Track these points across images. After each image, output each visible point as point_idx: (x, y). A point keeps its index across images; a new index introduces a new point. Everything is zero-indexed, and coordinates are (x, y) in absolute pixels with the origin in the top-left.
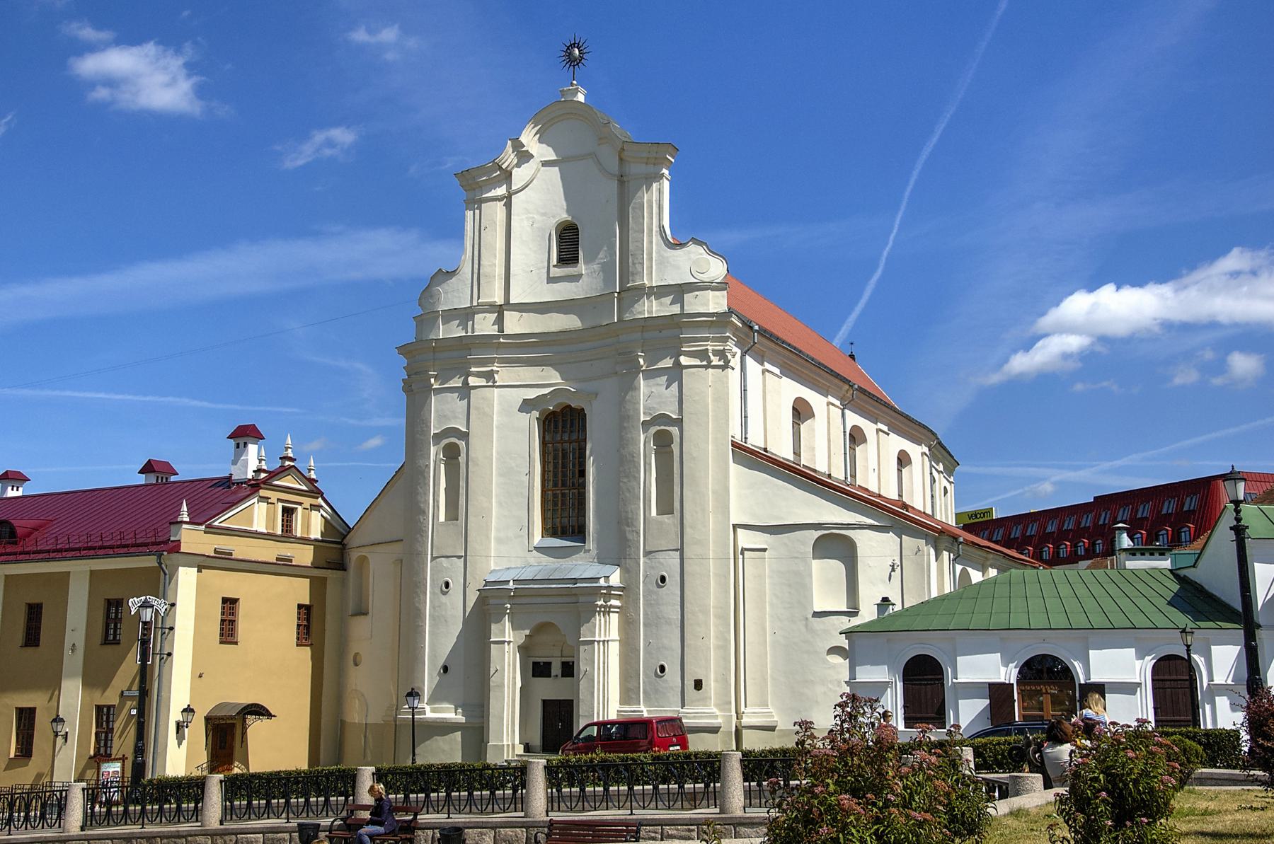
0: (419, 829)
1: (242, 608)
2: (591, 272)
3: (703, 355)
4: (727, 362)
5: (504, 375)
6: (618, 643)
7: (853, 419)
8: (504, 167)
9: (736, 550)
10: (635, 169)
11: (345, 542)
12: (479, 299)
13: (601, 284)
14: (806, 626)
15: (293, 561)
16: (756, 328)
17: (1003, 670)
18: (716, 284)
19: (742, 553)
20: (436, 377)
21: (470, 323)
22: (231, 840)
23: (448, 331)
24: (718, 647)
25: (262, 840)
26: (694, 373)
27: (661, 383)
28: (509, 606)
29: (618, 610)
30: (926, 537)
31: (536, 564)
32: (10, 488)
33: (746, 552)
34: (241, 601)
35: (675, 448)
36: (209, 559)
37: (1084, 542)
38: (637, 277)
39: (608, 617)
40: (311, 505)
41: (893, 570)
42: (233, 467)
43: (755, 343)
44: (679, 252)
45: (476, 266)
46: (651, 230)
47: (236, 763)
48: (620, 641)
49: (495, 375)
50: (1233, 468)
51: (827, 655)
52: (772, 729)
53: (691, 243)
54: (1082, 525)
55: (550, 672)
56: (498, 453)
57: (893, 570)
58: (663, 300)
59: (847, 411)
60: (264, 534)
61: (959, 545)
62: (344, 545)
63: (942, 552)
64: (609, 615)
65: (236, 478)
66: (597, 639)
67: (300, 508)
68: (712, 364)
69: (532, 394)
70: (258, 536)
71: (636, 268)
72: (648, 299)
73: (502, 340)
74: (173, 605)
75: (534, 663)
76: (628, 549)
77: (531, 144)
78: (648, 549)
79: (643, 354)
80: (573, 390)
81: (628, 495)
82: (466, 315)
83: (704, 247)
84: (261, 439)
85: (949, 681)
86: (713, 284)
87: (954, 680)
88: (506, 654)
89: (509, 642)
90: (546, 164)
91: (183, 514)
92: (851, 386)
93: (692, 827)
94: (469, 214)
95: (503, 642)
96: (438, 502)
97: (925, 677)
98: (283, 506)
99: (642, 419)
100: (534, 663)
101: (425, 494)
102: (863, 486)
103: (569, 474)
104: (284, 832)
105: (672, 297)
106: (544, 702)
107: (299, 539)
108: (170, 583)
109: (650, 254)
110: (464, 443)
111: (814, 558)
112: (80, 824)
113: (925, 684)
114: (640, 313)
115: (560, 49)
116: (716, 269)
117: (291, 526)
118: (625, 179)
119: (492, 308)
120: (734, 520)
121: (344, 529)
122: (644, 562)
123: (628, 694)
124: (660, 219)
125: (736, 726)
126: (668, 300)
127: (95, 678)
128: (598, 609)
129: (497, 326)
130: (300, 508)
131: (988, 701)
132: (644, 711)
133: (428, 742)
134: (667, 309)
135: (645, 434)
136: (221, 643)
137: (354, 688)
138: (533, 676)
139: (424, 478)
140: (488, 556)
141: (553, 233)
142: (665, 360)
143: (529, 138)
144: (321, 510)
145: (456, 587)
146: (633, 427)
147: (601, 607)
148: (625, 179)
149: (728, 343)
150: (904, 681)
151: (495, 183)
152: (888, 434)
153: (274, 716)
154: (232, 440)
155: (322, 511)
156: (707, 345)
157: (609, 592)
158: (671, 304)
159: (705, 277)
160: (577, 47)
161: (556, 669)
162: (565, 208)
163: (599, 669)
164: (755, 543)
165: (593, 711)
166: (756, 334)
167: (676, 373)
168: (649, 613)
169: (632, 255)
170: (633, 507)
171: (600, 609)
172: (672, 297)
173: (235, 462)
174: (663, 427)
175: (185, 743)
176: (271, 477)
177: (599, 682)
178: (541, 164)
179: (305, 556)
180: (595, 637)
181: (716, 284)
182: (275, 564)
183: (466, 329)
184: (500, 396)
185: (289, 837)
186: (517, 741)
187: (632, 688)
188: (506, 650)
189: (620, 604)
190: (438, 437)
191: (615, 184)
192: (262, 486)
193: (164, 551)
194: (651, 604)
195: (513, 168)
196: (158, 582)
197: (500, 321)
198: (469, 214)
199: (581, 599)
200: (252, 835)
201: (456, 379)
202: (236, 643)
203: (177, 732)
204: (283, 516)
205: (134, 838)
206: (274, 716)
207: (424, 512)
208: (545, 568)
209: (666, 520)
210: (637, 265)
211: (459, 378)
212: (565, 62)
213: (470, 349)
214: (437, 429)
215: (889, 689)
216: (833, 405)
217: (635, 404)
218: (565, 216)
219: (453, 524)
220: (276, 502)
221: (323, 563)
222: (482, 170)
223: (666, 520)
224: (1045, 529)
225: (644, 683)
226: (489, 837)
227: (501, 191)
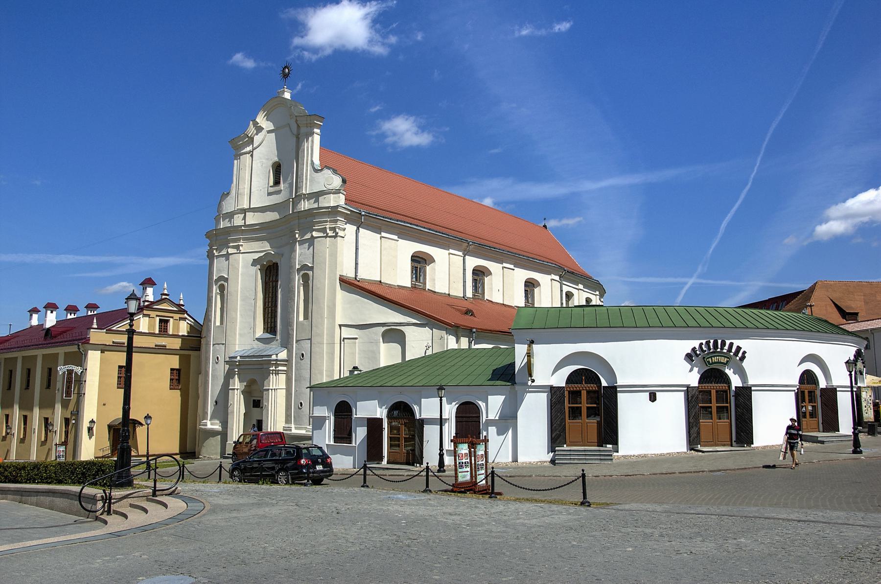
3: (324, 230)
5: (245, 246)
6: (285, 390)
7: (473, 262)
8: (249, 135)
13: (289, 195)
17: (379, 410)
28: (236, 370)
32: (69, 314)
33: (345, 340)
38: (301, 189)
44: (319, 174)
46: (307, 163)
49: (241, 247)
50: (133, 292)
56: (241, 288)
58: (311, 201)
63: (460, 338)
66: (271, 388)
68: (329, 235)
69: (256, 256)
72: (307, 201)
73: (243, 228)
78: (297, 339)
88: (236, 396)
89: (237, 389)
90: (269, 132)
94: (236, 162)
95: (234, 389)
97: (344, 414)
98: (160, 319)
100: (254, 401)
102: (489, 299)
105: (314, 199)
107: (171, 335)
109: (306, 176)
113: (344, 418)
114: (300, 209)
117: (166, 329)
122: (296, 346)
126: (312, 201)
127: (65, 405)
130: (171, 320)
133: (208, 440)
138: (253, 407)
143: (261, 119)
147: (273, 370)
149: (338, 223)
150: (335, 415)
152: (514, 270)
155: (187, 321)
157: (277, 363)
159: (330, 187)
162: (276, 154)
172: (314, 199)
174: (306, 272)
175: (94, 438)
176: (151, 304)
179: (176, 344)
180: (269, 387)
183: (231, 223)
184: (243, 258)
192: (145, 309)
195: (254, 136)
196: (80, 359)
198: (236, 162)
203: (89, 432)
204: (159, 324)
218: (276, 159)
220: (155, 316)
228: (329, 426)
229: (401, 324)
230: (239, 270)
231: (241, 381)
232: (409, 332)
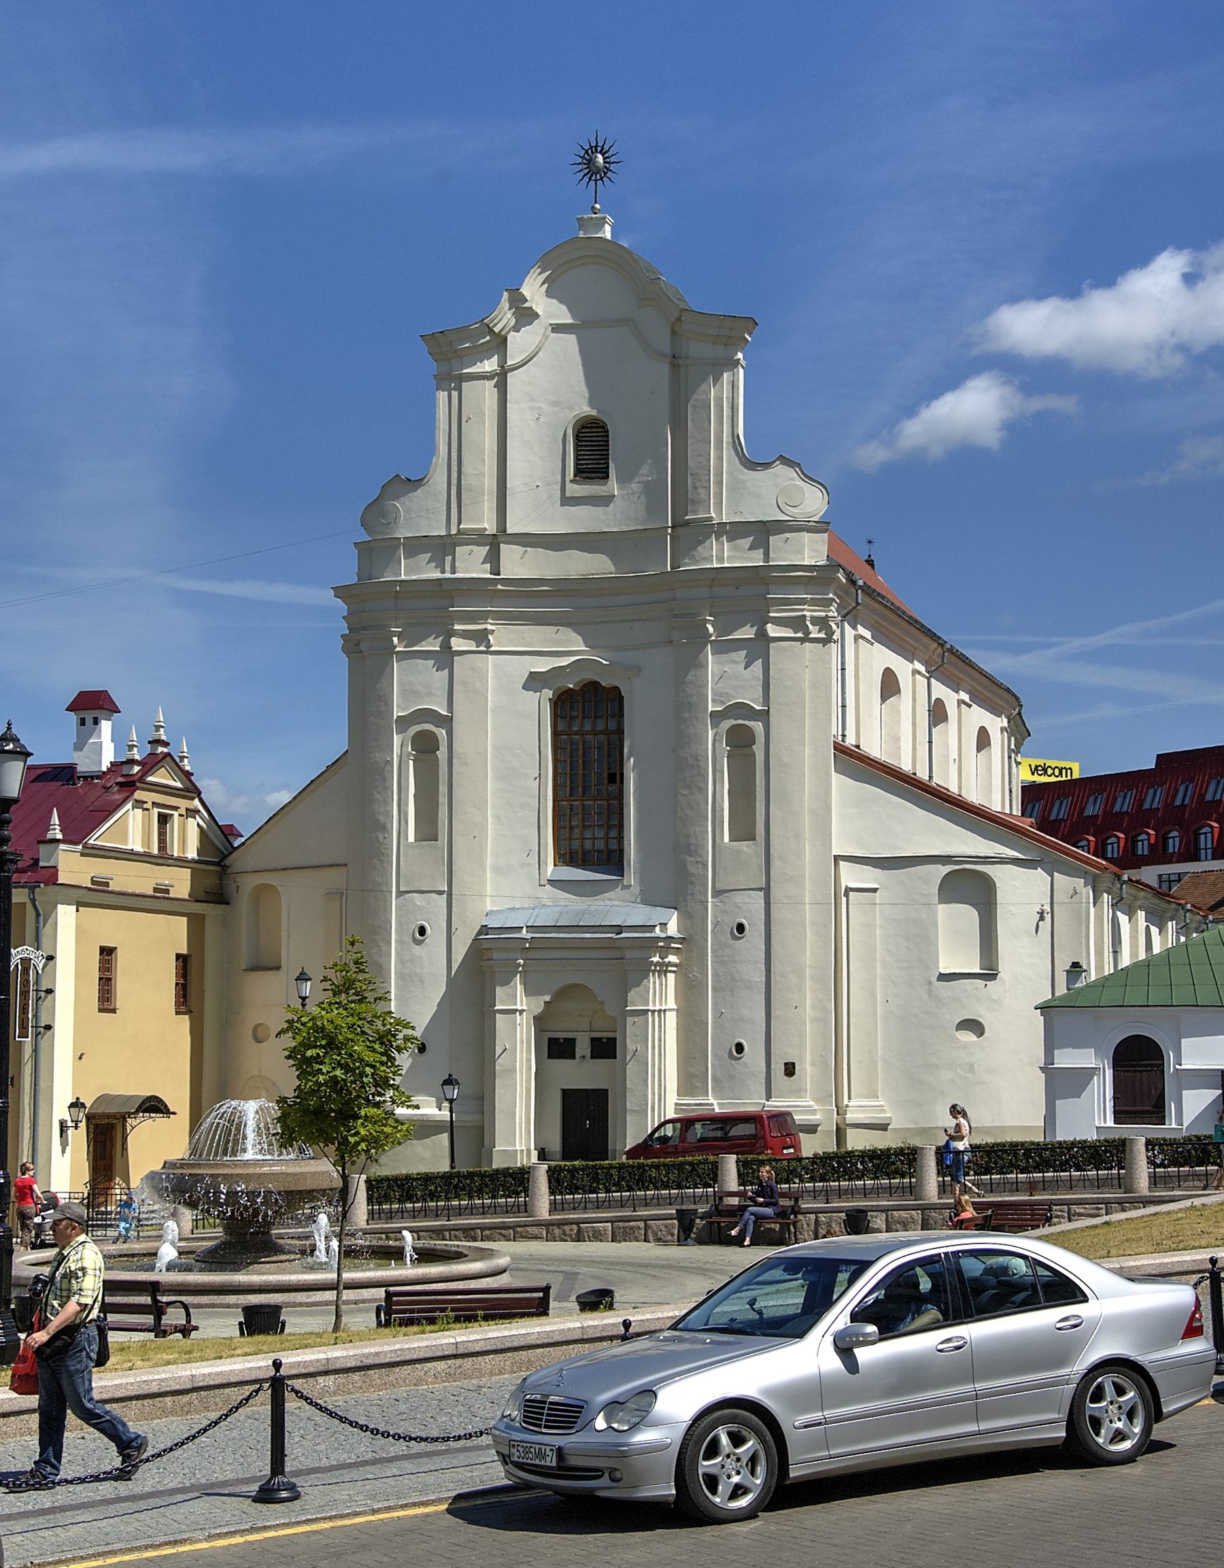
0: (802, 1213)
1: (122, 961)
2: (628, 494)
3: (798, 623)
4: (830, 633)
5: (502, 636)
7: (940, 690)
8: (496, 330)
9: (838, 890)
10: (696, 349)
11: (227, 862)
12: (459, 523)
14: (929, 992)
15: (171, 892)
16: (861, 583)
18: (814, 524)
19: (846, 895)
20: (399, 635)
21: (449, 559)
22: (571, 1230)
23: (408, 570)
24: (815, 1020)
25: (610, 1229)
26: (785, 649)
27: (737, 659)
29: (675, 969)
30: (1084, 874)
31: (551, 904)
33: (851, 893)
34: (118, 949)
35: (759, 750)
36: (91, 893)
37: (1148, 834)
39: (664, 979)
40: (187, 809)
41: (1042, 918)
42: (76, 754)
43: (858, 604)
44: (760, 475)
45: (454, 475)
47: (118, 1180)
48: (677, 1010)
49: (490, 637)
50: (9, 728)
51: (957, 1030)
52: (883, 1127)
53: (778, 462)
54: (1146, 806)
55: (574, 1051)
56: (494, 747)
57: (1042, 918)
58: (739, 542)
59: (933, 680)
60: (138, 854)
61: (1122, 885)
62: (225, 868)
64: (665, 976)
65: (83, 769)
66: (651, 1008)
67: (176, 814)
68: (811, 636)
70: (107, 854)
71: (698, 494)
73: (500, 587)
74: (51, 958)
75: (550, 1040)
76: (690, 887)
77: (536, 298)
78: (719, 886)
79: (712, 619)
80: (605, 662)
81: (689, 812)
82: (442, 548)
83: (797, 469)
84: (116, 712)
85: (1170, 1066)
86: (811, 524)
87: (1178, 1067)
88: (518, 1027)
89: (521, 1012)
90: (557, 328)
91: (55, 829)
92: (942, 646)
93: (1101, 1206)
94: (442, 396)
95: (514, 1011)
96: (406, 814)
99: (710, 709)
101: (386, 802)
103: (593, 778)
104: (638, 1221)
105: (752, 538)
106: (565, 1093)
108: (44, 926)
110: (444, 732)
111: (943, 900)
112: (365, 1217)
115: (573, 155)
116: (813, 502)
118: (681, 362)
119: (480, 538)
120: (835, 852)
121: (221, 843)
123: (690, 1081)
124: (733, 425)
125: (837, 1124)
126: (746, 542)
128: (653, 968)
129: (489, 565)
131: (1221, 1091)
132: (716, 1105)
134: (745, 555)
135: (715, 730)
136: (100, 1010)
137: (257, 1073)
139: (384, 779)
140: (483, 896)
141: (570, 432)
142: (744, 629)
143: (533, 289)
144: (197, 816)
145: (437, 934)
146: (697, 718)
147: (658, 963)
148: (681, 362)
151: (482, 353)
153: (174, 1113)
154: (73, 713)
156: (803, 610)
158: (749, 549)
160: (600, 153)
161: (583, 1047)
162: (587, 395)
163: (653, 1048)
164: (863, 882)
165: (647, 1104)
166: (860, 591)
167: (760, 648)
168: (721, 974)
169: (691, 474)
170: (697, 829)
171: (655, 967)
172: (752, 538)
173: (79, 747)
175: (68, 1149)
177: (653, 1065)
178: (550, 328)
179: (180, 883)
180: (648, 1005)
181: (814, 524)
182: (89, 889)
184: (496, 666)
185: (643, 1225)
186: (533, 1147)
187: (696, 1073)
188: (518, 1022)
189: (678, 961)
190: (404, 723)
191: (665, 368)
192: (138, 784)
193: (40, 882)
194: (723, 962)
195: (508, 332)
197: (494, 558)
198: (442, 396)
199: (628, 954)
200: (599, 1224)
201: (431, 639)
202: (114, 1011)
203: (61, 1136)
205: (446, 1230)
206: (174, 1113)
207: (385, 828)
208: (565, 909)
209: (745, 849)
210: (699, 490)
211: (434, 639)
212: (582, 174)
213: (453, 597)
214: (403, 710)
215: (1095, 1077)
216: (919, 673)
217: (700, 687)
218: (586, 410)
219: (430, 846)
221: (203, 897)
222: (463, 332)
223: (745, 849)
224: (1083, 809)
225: (712, 1065)
226: (881, 1220)
227: (490, 365)
228: (1102, 1089)
229: (986, 860)
230: (487, 697)
231: (528, 992)
232: (999, 874)
